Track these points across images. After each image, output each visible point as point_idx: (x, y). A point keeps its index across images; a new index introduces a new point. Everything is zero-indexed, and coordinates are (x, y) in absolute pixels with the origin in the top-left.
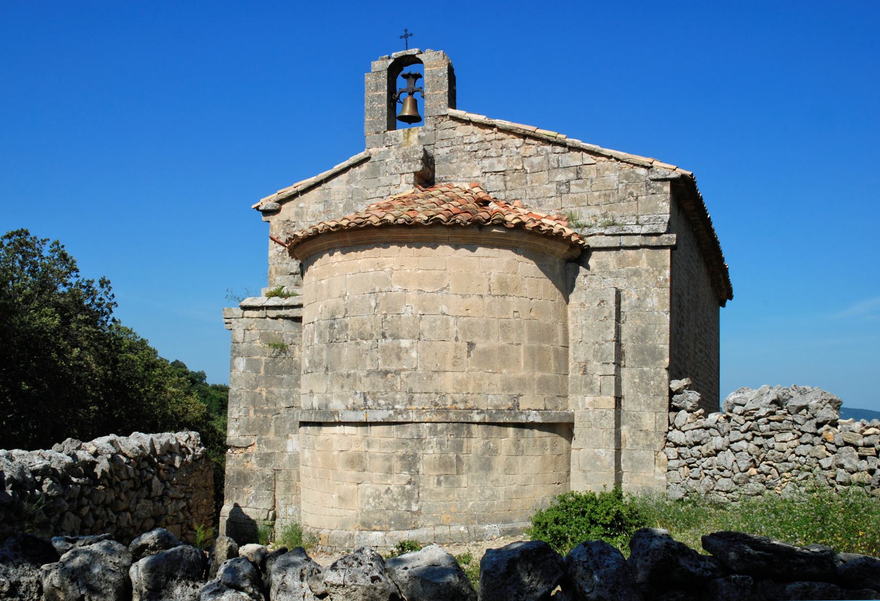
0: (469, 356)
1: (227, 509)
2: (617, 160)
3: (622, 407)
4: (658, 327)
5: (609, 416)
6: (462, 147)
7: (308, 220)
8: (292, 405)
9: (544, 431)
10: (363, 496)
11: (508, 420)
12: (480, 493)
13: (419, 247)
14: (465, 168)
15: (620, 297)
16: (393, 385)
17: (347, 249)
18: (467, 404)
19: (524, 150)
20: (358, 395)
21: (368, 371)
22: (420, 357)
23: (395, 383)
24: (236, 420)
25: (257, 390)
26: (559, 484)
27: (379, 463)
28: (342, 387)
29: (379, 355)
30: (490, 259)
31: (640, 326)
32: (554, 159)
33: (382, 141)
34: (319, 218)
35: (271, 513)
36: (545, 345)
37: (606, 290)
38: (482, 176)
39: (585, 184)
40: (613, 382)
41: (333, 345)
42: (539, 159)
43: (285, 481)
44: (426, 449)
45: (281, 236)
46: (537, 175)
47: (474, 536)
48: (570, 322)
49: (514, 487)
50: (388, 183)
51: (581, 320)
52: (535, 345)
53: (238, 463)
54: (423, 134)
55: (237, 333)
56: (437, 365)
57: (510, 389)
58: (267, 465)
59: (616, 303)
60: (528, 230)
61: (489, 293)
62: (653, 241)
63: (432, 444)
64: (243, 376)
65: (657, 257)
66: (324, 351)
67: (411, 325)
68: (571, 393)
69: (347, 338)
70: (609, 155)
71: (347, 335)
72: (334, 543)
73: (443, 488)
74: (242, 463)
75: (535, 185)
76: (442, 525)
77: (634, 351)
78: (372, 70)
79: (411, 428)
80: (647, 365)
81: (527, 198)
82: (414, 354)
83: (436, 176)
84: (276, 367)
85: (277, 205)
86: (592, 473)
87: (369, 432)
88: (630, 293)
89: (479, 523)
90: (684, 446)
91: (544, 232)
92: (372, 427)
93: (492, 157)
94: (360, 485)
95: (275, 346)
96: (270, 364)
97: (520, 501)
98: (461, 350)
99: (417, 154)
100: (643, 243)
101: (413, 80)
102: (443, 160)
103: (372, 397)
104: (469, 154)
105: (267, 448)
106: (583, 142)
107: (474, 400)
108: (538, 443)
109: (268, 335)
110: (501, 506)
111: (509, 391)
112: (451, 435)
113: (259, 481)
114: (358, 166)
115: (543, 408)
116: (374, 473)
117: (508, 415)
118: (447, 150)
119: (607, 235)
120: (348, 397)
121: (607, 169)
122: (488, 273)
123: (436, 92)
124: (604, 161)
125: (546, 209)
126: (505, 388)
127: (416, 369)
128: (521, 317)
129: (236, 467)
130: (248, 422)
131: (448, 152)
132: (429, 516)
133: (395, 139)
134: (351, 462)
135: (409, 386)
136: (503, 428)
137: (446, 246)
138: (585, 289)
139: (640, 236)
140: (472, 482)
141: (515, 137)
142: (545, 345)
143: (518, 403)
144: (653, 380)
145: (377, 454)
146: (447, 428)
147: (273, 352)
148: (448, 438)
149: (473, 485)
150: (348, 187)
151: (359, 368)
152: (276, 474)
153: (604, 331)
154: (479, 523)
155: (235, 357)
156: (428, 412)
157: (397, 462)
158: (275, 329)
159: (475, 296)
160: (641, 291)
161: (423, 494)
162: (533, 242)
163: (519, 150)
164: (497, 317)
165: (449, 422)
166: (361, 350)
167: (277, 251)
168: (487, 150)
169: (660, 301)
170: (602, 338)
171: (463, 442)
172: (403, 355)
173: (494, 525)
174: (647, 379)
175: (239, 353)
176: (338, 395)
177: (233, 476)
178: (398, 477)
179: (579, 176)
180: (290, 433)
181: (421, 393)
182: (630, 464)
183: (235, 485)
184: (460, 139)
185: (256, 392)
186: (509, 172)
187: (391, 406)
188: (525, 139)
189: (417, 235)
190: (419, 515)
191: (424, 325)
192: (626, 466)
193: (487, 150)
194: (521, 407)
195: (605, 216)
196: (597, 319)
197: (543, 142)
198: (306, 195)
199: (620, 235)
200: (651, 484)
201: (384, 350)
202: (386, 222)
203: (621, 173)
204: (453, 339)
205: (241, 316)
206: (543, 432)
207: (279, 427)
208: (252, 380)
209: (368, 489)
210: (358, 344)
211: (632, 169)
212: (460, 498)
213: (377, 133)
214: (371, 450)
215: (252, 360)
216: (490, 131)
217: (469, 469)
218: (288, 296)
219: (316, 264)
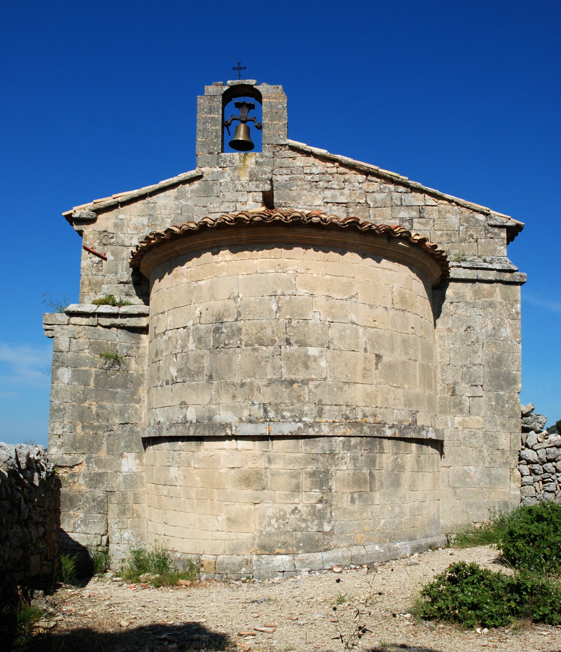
2: (458, 204)
4: (511, 355)
5: (479, 435)
7: (130, 232)
8: (127, 421)
10: (262, 517)
13: (326, 251)
16: (300, 396)
18: (377, 418)
20: (257, 407)
21: (270, 380)
22: (330, 366)
23: (302, 393)
24: (59, 437)
25: (86, 404)
28: (234, 397)
29: (282, 363)
31: (495, 353)
33: (216, 162)
34: (142, 231)
35: (105, 538)
38: (324, 206)
39: (428, 223)
41: (219, 352)
42: (382, 195)
43: (119, 503)
44: (340, 465)
45: (97, 246)
46: (381, 210)
47: (389, 555)
50: (234, 199)
51: (448, 343)
55: (60, 341)
56: (347, 376)
57: (410, 405)
58: (98, 485)
62: (507, 277)
63: (346, 460)
65: (509, 292)
66: (205, 358)
69: (241, 343)
71: (241, 340)
72: (224, 569)
73: (357, 506)
75: (379, 219)
76: (356, 545)
78: (206, 94)
79: (322, 442)
80: (502, 389)
82: (323, 364)
83: (275, 200)
84: (109, 379)
85: (94, 215)
86: (462, 489)
88: (486, 322)
90: (537, 463)
93: (334, 189)
94: (257, 505)
95: (107, 357)
96: (102, 376)
98: (369, 362)
100: (498, 278)
101: (247, 110)
103: (275, 408)
104: (310, 184)
105: (98, 468)
107: (382, 414)
111: (410, 407)
114: (189, 183)
116: (277, 492)
118: (286, 178)
119: (464, 268)
120: (242, 409)
121: (449, 212)
122: (391, 286)
123: (274, 122)
126: (406, 403)
127: (325, 379)
131: (288, 179)
132: (343, 536)
134: (246, 480)
135: (318, 397)
139: (495, 272)
140: (384, 499)
144: (508, 403)
145: (282, 471)
146: (361, 442)
147: (105, 364)
148: (362, 453)
149: (384, 502)
150: (177, 203)
151: (257, 376)
153: (471, 355)
154: (390, 541)
155: (58, 367)
156: (342, 425)
158: (108, 338)
159: (380, 307)
160: (495, 321)
161: (336, 513)
164: (399, 331)
166: (259, 357)
167: (92, 261)
168: (329, 181)
169: (513, 331)
171: (376, 457)
172: (311, 364)
174: (503, 402)
175: (62, 363)
179: (421, 216)
180: (125, 451)
181: (331, 405)
184: (301, 169)
185: (84, 407)
187: (298, 418)
189: (328, 238)
191: (333, 333)
193: (329, 181)
194: (419, 423)
196: (464, 344)
197: (385, 181)
198: (126, 207)
200: (506, 498)
201: (289, 357)
202: (298, 219)
203: (462, 217)
204: (362, 350)
205: (66, 323)
207: (112, 445)
209: (269, 509)
211: (471, 215)
213: (210, 153)
214: (273, 466)
215: (79, 371)
216: (332, 165)
217: (381, 485)
218: (121, 304)
219: (188, 264)
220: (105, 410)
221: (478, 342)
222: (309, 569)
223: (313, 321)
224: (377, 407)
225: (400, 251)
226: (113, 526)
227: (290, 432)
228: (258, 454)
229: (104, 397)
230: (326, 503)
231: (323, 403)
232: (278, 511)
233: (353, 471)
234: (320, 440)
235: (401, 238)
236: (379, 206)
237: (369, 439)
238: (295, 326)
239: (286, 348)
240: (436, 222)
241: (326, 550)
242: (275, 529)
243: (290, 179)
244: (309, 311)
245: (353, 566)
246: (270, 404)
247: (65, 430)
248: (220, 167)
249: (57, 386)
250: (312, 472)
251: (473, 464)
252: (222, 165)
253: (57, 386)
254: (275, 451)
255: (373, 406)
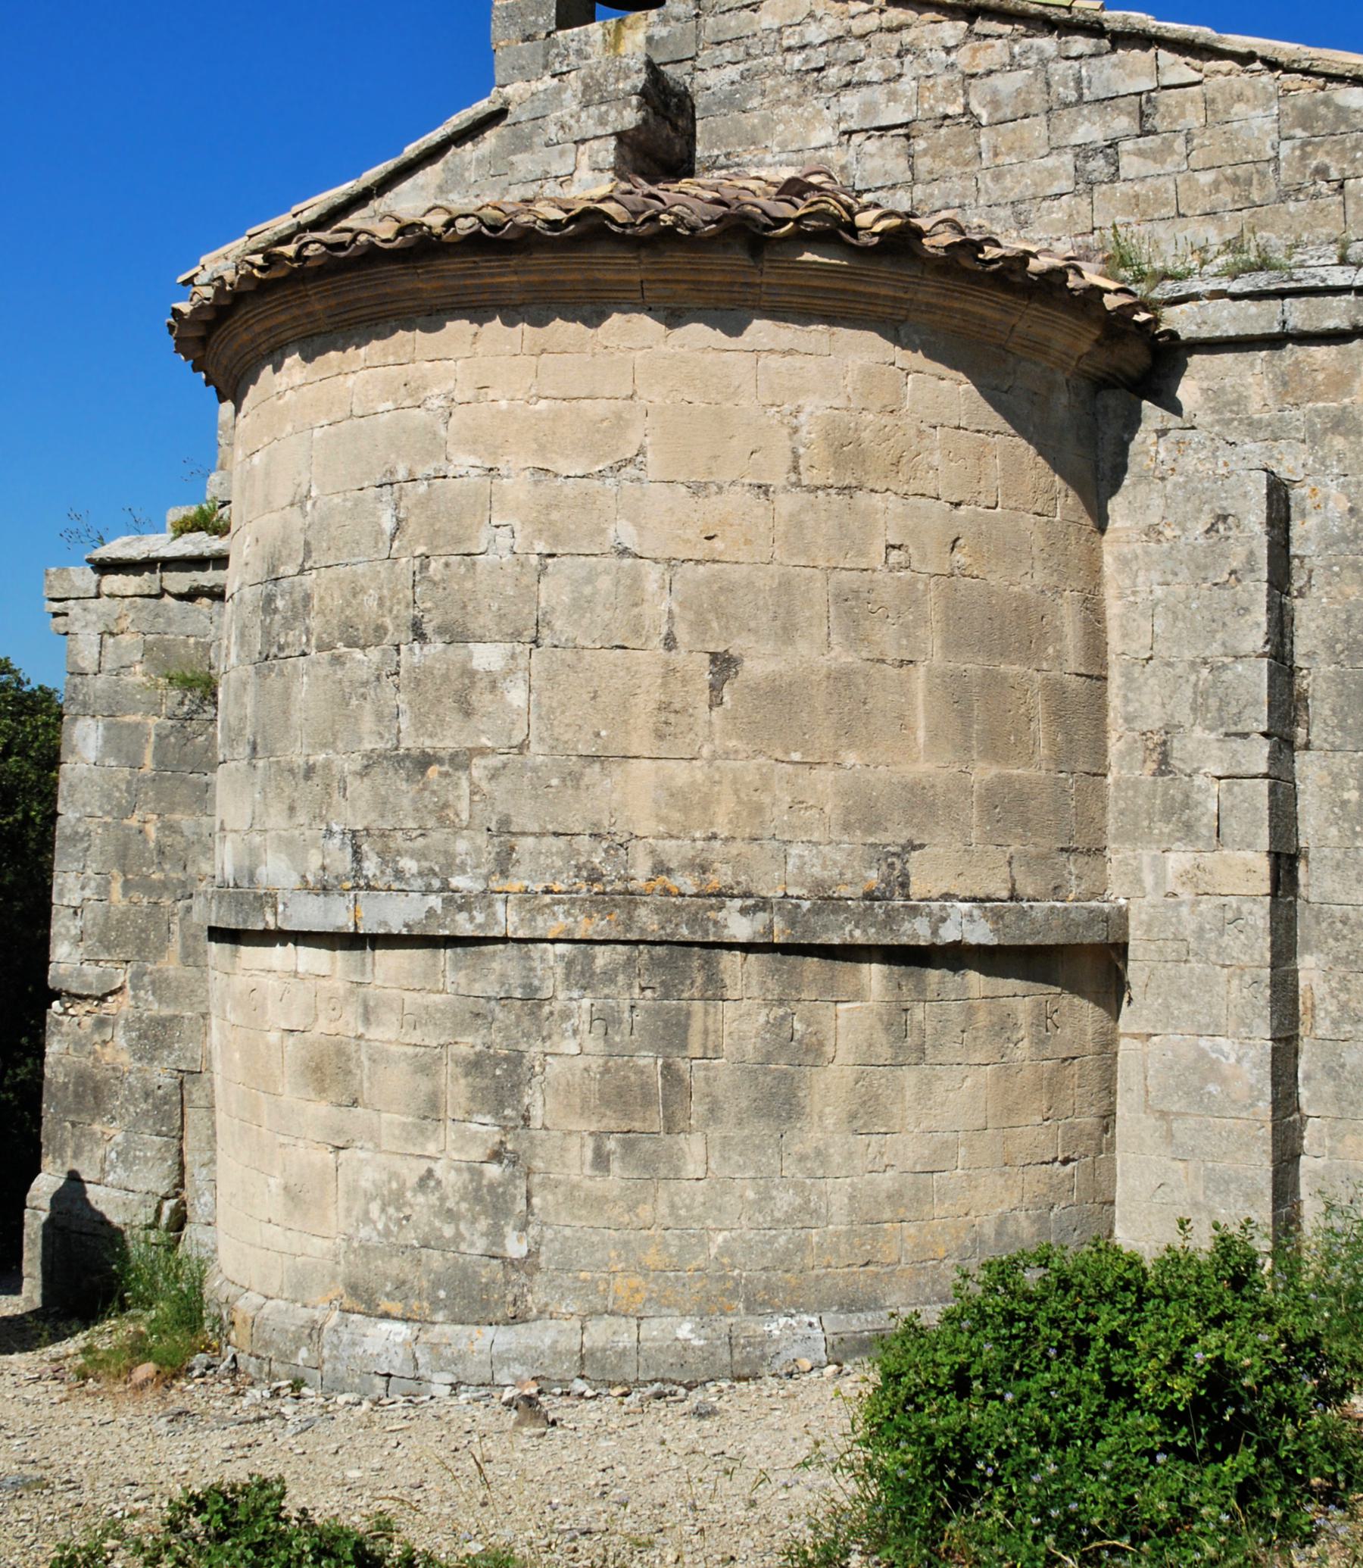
0: (715, 702)
1: (45, 1185)
2: (1272, 65)
3: (1302, 890)
5: (1251, 920)
6: (779, 59)
9: (1006, 976)
11: (859, 937)
12: (755, 1202)
13: (539, 322)
14: (787, 123)
15: (1288, 507)
16: (446, 805)
17: (318, 341)
18: (709, 876)
19: (969, 54)
20: (337, 840)
21: (367, 756)
22: (539, 704)
23: (451, 797)
24: (75, 913)
25: (133, 822)
26: (1066, 1161)
27: (397, 1079)
28: (292, 809)
30: (797, 361)
32: (1064, 76)
33: (541, 61)
36: (1011, 669)
37: (1234, 478)
38: (840, 144)
39: (1168, 148)
40: (1263, 802)
41: (271, 669)
42: (1019, 78)
44: (555, 1038)
46: (1013, 130)
48: (1109, 593)
49: (887, 1181)
50: (539, 173)
51: (1148, 583)
52: (973, 666)
53: (79, 1045)
54: (661, 32)
55: (81, 645)
56: (597, 735)
58: (157, 1053)
59: (1271, 522)
60: (935, 257)
61: (793, 478)
63: (575, 1021)
64: (96, 776)
67: (510, 591)
68: (1115, 839)
69: (308, 640)
70: (1244, 50)
74: (89, 1047)
76: (612, 1313)
77: (1340, 695)
79: (501, 959)
81: (981, 202)
82: (516, 696)
83: (700, 151)
84: (189, 748)
86: (1191, 1122)
87: (369, 968)
88: (1322, 491)
89: (749, 1310)
91: (995, 266)
92: (378, 952)
93: (869, 83)
94: (342, 1153)
96: (172, 740)
97: (910, 1229)
98: (685, 682)
99: (627, 77)
102: (721, 104)
103: (379, 846)
104: (800, 80)
106: (1158, 19)
108: (982, 1018)
109: (166, 650)
110: (835, 1250)
111: (868, 831)
112: (643, 989)
113: (136, 1106)
114: (472, 139)
115: (1005, 894)
116: (384, 1115)
117: (861, 919)
118: (732, 72)
119: (1235, 297)
121: (1240, 97)
122: (787, 408)
124: (1229, 74)
125: (1042, 235)
126: (852, 818)
127: (522, 747)
128: (915, 565)
129: (74, 1057)
130: (107, 918)
131: (737, 78)
132: (567, 1280)
133: (579, 52)
136: (839, 965)
137: (635, 317)
138: (1163, 479)
139: (1352, 297)
141: (940, 17)
142: (1011, 669)
143: (906, 875)
145: (393, 1048)
146: (630, 961)
147: (182, 703)
149: (727, 1172)
151: (340, 745)
152: (187, 1086)
153: (1227, 619)
154: (749, 1310)
156: (559, 902)
157: (455, 1079)
158: (189, 630)
159: (738, 488)
161: (544, 1199)
162: (957, 305)
163: (953, 56)
164: (822, 564)
165: (637, 943)
168: (854, 62)
170: (1224, 644)
171: (689, 1015)
172: (481, 699)
173: (806, 1318)
175: (85, 705)
176: (280, 837)
177: (65, 1085)
178: (462, 1135)
179: (1148, 126)
182: (1329, 1088)
183: (67, 1111)
184: (773, 37)
185: (130, 828)
186: (922, 125)
188: (971, 22)
189: (535, 278)
190: (530, 1275)
191: (553, 592)
192: (1316, 1098)
193: (854, 62)
194: (916, 889)
195: (1233, 246)
196: (1205, 579)
197: (1028, 27)
199: (1282, 294)
202: (418, 233)
204: (657, 642)
206: (1000, 981)
208: (120, 790)
210: (337, 660)
211: (1321, 94)
212: (678, 1218)
213: (528, 38)
214: (374, 1033)
217: (714, 1111)
220: (179, 838)
221: (1252, 571)
222: (451, 1379)
223: (491, 557)
224: (714, 837)
225: (816, 283)
226: (196, 1171)
227: (406, 925)
228: (341, 992)
229: (177, 799)
230: (514, 1163)
231: (514, 829)
232: (385, 1177)
233: (601, 1061)
234: (495, 952)
235: (803, 238)
236: (1009, 116)
237: (659, 950)
238: (437, 578)
239: (411, 649)
240: (1196, 142)
241: (514, 1320)
242: (379, 1234)
243: (742, 78)
244: (481, 523)
245: (579, 1386)
246: (368, 835)
247: (88, 893)
248: (553, 76)
249: (73, 769)
250: (472, 1057)
251: (1231, 1029)
252: (557, 68)
253: (73, 769)
254: (378, 982)
255: (698, 835)
